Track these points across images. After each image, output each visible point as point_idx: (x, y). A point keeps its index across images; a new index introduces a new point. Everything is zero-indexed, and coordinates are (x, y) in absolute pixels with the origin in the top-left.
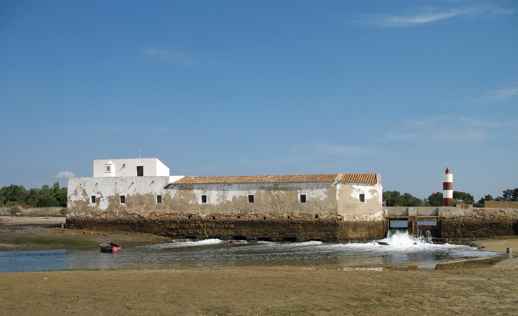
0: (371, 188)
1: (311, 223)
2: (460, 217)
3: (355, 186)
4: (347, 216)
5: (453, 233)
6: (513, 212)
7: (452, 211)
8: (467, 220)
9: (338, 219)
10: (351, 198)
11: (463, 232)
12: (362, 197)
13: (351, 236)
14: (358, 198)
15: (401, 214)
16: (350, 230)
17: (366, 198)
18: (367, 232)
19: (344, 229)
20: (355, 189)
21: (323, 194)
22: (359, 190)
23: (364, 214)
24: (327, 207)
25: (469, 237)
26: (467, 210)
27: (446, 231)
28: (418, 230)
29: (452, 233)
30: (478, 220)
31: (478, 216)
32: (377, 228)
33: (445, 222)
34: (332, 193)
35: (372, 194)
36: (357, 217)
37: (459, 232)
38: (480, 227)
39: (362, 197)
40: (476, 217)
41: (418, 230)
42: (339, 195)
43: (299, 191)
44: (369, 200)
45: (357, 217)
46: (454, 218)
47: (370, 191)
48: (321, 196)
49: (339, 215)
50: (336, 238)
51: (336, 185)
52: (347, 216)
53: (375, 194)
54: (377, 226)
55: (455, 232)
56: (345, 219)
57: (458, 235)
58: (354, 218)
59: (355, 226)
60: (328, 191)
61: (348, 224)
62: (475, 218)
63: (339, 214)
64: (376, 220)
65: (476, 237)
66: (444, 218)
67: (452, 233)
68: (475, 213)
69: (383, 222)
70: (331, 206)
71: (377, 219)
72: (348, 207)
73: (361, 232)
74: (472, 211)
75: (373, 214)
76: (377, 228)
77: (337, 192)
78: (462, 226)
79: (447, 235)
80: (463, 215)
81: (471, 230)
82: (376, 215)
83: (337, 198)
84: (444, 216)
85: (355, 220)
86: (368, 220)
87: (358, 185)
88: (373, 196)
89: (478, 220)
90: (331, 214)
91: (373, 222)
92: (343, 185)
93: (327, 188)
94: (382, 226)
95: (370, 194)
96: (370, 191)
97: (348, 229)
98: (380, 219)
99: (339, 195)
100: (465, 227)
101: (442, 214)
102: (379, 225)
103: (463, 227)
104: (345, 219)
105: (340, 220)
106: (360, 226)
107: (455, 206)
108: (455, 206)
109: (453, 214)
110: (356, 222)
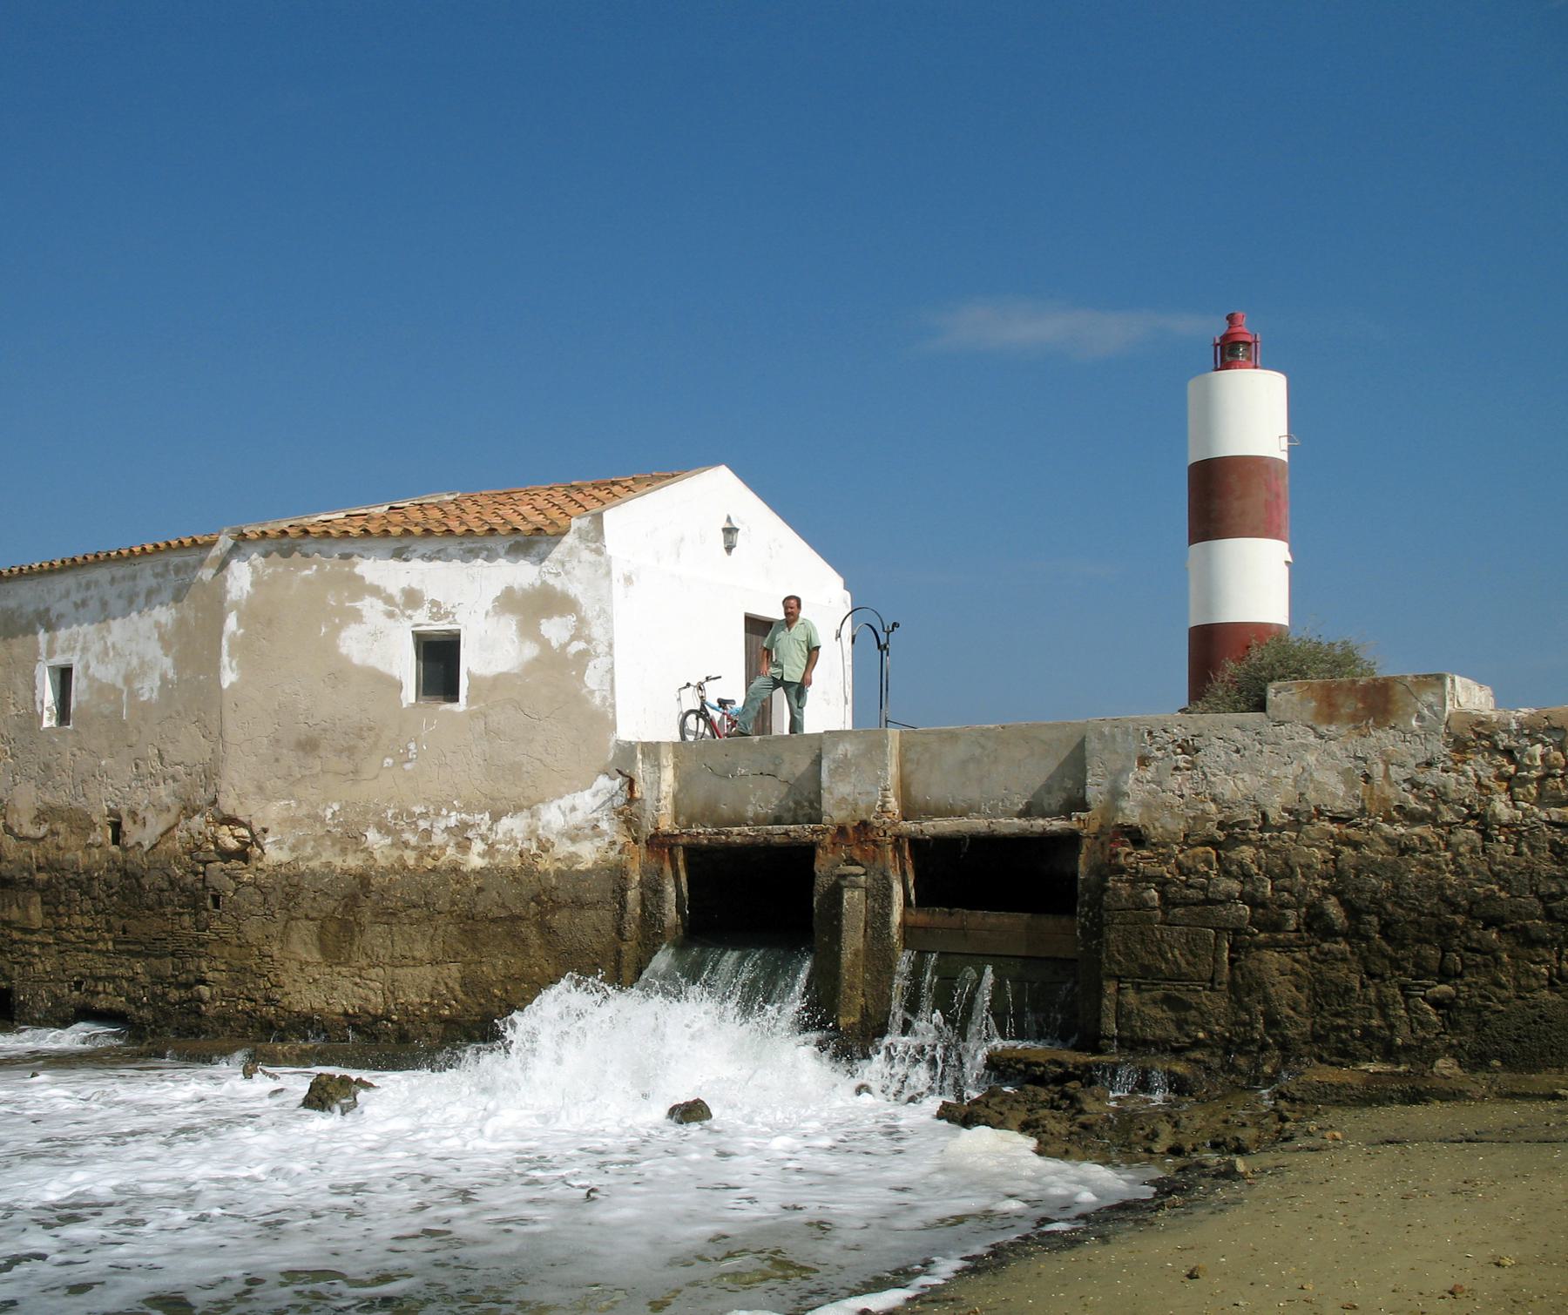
0: (522, 573)
1: (83, 883)
2: (1298, 818)
3: (375, 569)
4: (286, 827)
5: (1216, 1003)
6: (24, 596)
7: (1214, 755)
8: (1377, 853)
9: (226, 855)
10: (340, 673)
11: (1324, 994)
12: (439, 659)
13: (304, 996)
14: (405, 666)
15: (769, 810)
16: (303, 946)
17: (471, 662)
18: (454, 970)
19: (252, 930)
20: (376, 591)
21: (154, 650)
22: (413, 598)
23: (439, 806)
24: (172, 754)
25: (1390, 1053)
26: (1384, 738)
27: (1146, 976)
28: (904, 962)
29: (1204, 997)
30: (1502, 849)
31: (1502, 808)
32: (545, 929)
33: (1139, 878)
34: (196, 647)
35: (528, 630)
36: (373, 837)
37: (1283, 991)
38: (1529, 941)
39: (439, 659)
40: (1484, 823)
41: (904, 962)
42: (242, 648)
43: (42, 637)
44: (499, 680)
45: (373, 837)
46: (1232, 833)
47: (509, 602)
48: (145, 667)
49: (231, 821)
50: (193, 1006)
51: (223, 565)
52: (294, 822)
53: (555, 630)
54: (559, 920)
55: (1244, 988)
56: (274, 853)
57: (1272, 1022)
58: (352, 839)
59: (351, 910)
60: (181, 622)
61: (288, 891)
62: (1468, 835)
63: (229, 805)
64: (545, 864)
65: (1476, 1061)
66: (1136, 837)
67: (1204, 997)
68: (1479, 766)
69: (617, 876)
70: (189, 747)
71: (563, 848)
72: (308, 746)
73: (399, 962)
74: (1438, 747)
75: (526, 805)
76: (545, 929)
77: (231, 623)
78: (1315, 921)
79: (1158, 1021)
80: (1336, 792)
81: (1422, 971)
82: (553, 817)
83: (228, 678)
84: (1131, 813)
85: (353, 862)
86: (475, 860)
87: (400, 554)
88: (531, 650)
89: (1502, 849)
90: (189, 810)
91: (523, 875)
92: (278, 566)
93: (177, 598)
94: (602, 918)
95: (509, 626)
96: (509, 602)
97: (285, 938)
98: (588, 854)
99: (242, 648)
100: (1354, 934)
101: (1116, 794)
102: (579, 904)
103: (1329, 932)
104: (274, 853)
105: (242, 855)
106: (388, 916)
107: (1261, 706)
108: (1261, 706)
109: (1228, 788)
110: (364, 880)
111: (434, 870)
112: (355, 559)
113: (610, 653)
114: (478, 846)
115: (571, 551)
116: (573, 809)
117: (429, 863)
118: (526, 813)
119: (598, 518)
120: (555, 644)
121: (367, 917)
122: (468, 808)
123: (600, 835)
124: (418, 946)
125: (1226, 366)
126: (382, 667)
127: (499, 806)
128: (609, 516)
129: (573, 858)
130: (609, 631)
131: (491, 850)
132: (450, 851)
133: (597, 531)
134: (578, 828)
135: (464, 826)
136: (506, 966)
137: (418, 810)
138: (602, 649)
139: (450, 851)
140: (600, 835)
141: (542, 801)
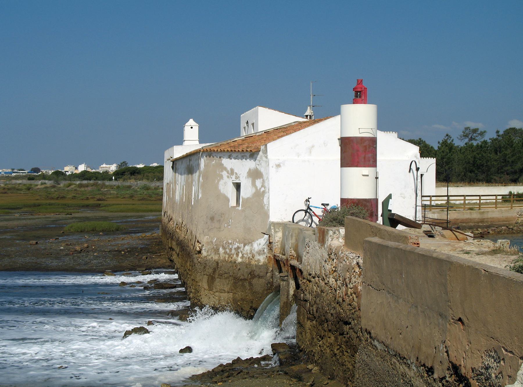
4: (490, 256)
56: (204, 253)
61: (205, 264)
76: (251, 284)
85: (216, 257)
91: (248, 265)
111: (231, 262)
112: (222, 158)
113: (269, 192)
114: (240, 255)
115: (261, 158)
116: (260, 244)
117: (230, 259)
118: (250, 245)
119: (266, 145)
120: (258, 188)
121: (216, 276)
122: (239, 242)
123: (264, 253)
124: (225, 286)
125: (355, 102)
126: (226, 195)
127: (246, 242)
128: (269, 145)
129: (259, 261)
130: (269, 184)
131: (242, 257)
132: (235, 256)
133: (265, 152)
134: (260, 251)
135: (238, 248)
136: (241, 295)
137: (230, 241)
138: (267, 190)
139: (235, 256)
140: (264, 253)
141: (254, 241)
